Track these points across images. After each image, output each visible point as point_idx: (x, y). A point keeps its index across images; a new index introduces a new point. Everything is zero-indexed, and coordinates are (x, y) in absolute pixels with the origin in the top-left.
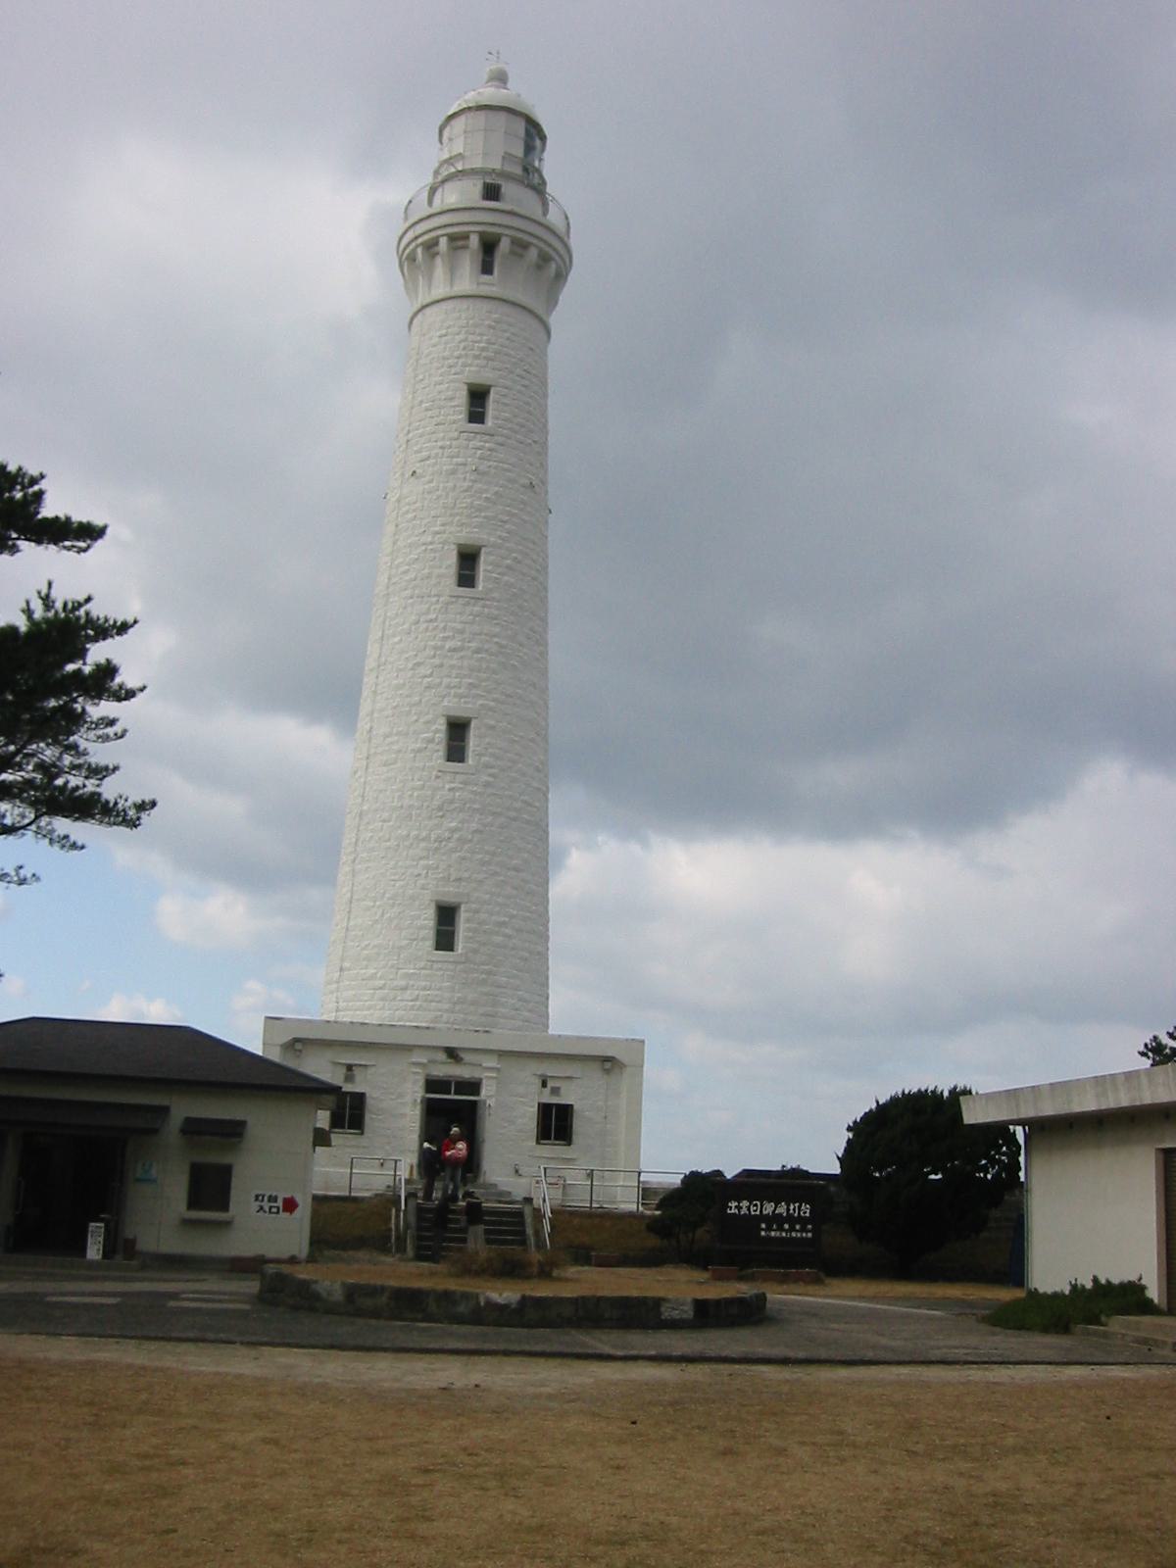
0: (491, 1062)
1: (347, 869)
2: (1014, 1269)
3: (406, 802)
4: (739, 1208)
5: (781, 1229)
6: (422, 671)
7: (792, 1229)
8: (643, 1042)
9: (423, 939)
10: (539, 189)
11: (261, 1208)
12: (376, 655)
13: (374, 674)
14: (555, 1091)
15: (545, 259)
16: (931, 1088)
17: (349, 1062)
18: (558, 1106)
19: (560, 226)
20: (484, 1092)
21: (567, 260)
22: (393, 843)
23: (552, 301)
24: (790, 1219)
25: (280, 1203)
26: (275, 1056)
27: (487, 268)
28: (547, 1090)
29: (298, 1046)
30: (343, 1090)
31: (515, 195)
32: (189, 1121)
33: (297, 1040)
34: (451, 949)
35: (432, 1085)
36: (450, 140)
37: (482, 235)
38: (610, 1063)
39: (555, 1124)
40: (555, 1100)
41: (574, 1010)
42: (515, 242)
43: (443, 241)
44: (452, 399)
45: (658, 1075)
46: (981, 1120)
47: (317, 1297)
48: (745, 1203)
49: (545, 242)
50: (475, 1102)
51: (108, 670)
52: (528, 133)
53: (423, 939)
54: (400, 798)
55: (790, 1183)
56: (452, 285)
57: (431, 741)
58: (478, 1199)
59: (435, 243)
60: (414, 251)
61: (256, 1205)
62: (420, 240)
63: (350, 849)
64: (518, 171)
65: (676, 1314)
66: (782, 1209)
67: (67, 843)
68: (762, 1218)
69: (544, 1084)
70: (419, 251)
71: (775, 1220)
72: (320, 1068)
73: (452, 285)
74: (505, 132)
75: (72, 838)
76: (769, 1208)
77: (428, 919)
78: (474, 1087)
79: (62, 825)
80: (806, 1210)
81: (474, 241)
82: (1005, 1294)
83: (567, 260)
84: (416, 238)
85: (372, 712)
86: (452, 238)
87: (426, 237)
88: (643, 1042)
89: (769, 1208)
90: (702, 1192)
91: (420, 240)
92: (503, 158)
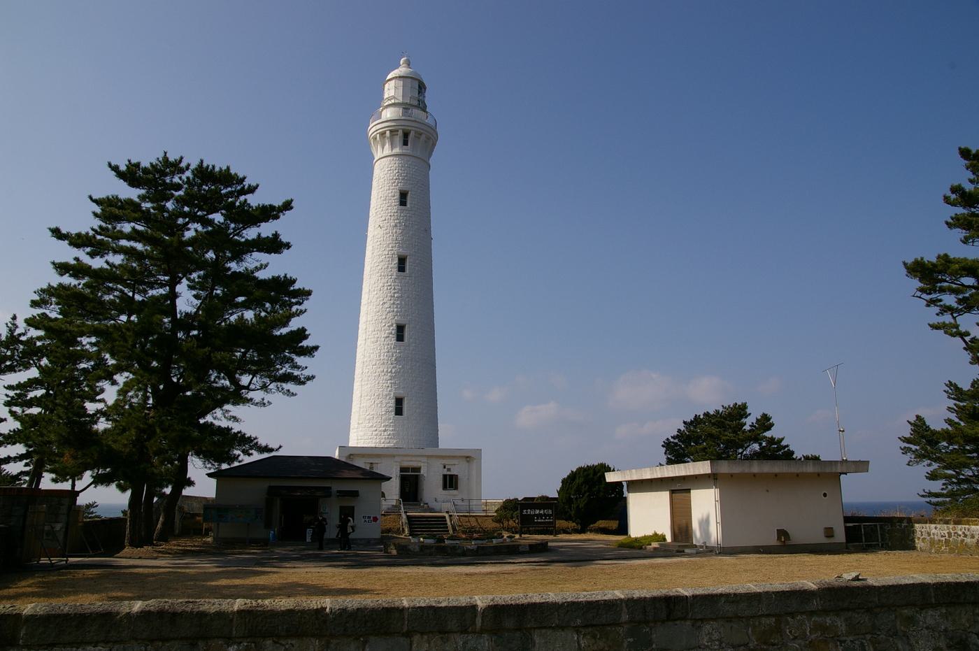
0: (425, 459)
1: (358, 384)
2: (623, 529)
3: (382, 358)
4: (527, 512)
5: (542, 519)
6: (386, 306)
7: (546, 518)
8: (481, 450)
9: (391, 411)
10: (424, 109)
11: (365, 521)
12: (366, 299)
13: (366, 307)
14: (449, 470)
15: (429, 138)
16: (282, 275)
17: (371, 462)
18: (450, 475)
19: (432, 123)
20: (422, 472)
21: (435, 136)
22: (377, 374)
23: (430, 156)
24: (545, 515)
25: (372, 519)
26: (344, 460)
27: (405, 143)
28: (446, 470)
29: (352, 457)
30: (38, 396)
31: (417, 113)
32: (338, 492)
33: (351, 455)
34: (401, 415)
35: (403, 469)
36: (389, 89)
37: (403, 130)
38: (470, 458)
39: (450, 482)
40: (449, 473)
41: (450, 436)
42: (416, 132)
43: (388, 133)
44: (394, 196)
45: (487, 464)
46: (612, 481)
47: (409, 550)
48: (529, 510)
49: (428, 132)
50: (417, 475)
51: (301, 334)
52: (419, 87)
53: (391, 411)
54: (380, 356)
55: (544, 502)
56: (392, 150)
57: (391, 333)
58: (432, 510)
59: (385, 133)
60: (376, 135)
61: (363, 520)
62: (378, 132)
63: (359, 376)
64: (416, 103)
65: (524, 550)
66: (542, 512)
67: (289, 393)
68: (535, 515)
69: (445, 467)
70: (378, 135)
71: (539, 516)
72: (359, 463)
73: (392, 150)
74: (411, 87)
75: (291, 391)
76: (537, 512)
77: (392, 403)
78: (418, 469)
79: (287, 386)
80: (550, 512)
81: (400, 133)
82: (621, 538)
83: (435, 136)
84: (377, 130)
85: (367, 321)
86: (391, 131)
87: (381, 130)
88: (481, 450)
89: (537, 512)
90: (511, 506)
91: (378, 132)
92: (411, 98)
